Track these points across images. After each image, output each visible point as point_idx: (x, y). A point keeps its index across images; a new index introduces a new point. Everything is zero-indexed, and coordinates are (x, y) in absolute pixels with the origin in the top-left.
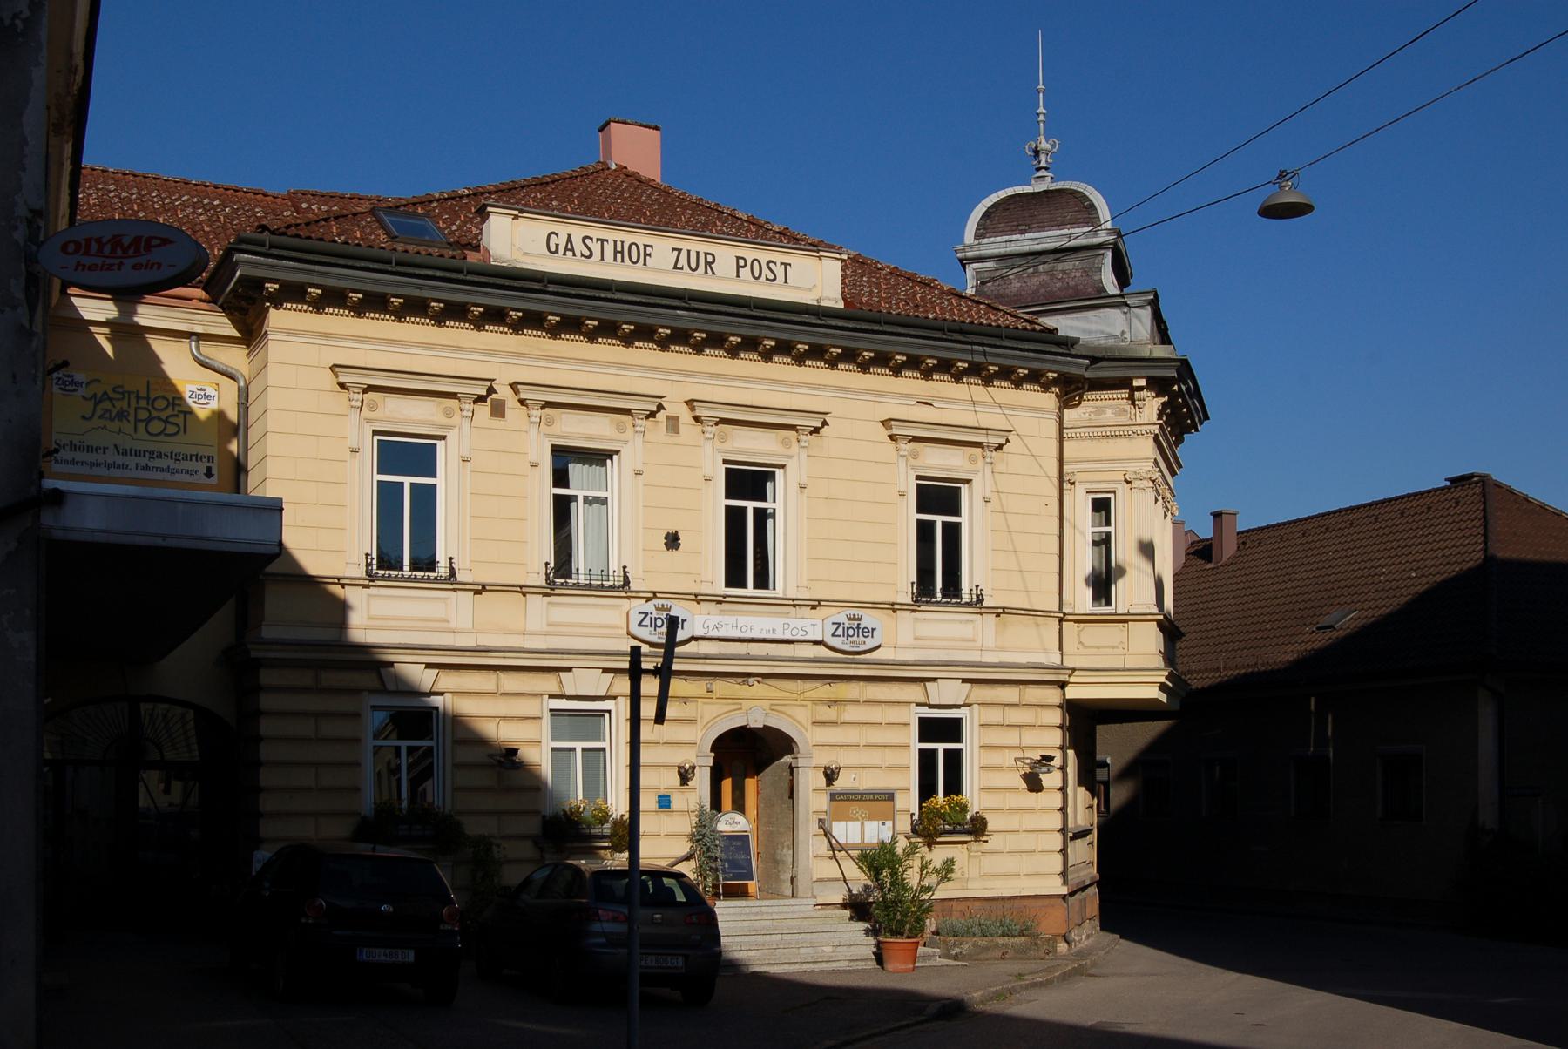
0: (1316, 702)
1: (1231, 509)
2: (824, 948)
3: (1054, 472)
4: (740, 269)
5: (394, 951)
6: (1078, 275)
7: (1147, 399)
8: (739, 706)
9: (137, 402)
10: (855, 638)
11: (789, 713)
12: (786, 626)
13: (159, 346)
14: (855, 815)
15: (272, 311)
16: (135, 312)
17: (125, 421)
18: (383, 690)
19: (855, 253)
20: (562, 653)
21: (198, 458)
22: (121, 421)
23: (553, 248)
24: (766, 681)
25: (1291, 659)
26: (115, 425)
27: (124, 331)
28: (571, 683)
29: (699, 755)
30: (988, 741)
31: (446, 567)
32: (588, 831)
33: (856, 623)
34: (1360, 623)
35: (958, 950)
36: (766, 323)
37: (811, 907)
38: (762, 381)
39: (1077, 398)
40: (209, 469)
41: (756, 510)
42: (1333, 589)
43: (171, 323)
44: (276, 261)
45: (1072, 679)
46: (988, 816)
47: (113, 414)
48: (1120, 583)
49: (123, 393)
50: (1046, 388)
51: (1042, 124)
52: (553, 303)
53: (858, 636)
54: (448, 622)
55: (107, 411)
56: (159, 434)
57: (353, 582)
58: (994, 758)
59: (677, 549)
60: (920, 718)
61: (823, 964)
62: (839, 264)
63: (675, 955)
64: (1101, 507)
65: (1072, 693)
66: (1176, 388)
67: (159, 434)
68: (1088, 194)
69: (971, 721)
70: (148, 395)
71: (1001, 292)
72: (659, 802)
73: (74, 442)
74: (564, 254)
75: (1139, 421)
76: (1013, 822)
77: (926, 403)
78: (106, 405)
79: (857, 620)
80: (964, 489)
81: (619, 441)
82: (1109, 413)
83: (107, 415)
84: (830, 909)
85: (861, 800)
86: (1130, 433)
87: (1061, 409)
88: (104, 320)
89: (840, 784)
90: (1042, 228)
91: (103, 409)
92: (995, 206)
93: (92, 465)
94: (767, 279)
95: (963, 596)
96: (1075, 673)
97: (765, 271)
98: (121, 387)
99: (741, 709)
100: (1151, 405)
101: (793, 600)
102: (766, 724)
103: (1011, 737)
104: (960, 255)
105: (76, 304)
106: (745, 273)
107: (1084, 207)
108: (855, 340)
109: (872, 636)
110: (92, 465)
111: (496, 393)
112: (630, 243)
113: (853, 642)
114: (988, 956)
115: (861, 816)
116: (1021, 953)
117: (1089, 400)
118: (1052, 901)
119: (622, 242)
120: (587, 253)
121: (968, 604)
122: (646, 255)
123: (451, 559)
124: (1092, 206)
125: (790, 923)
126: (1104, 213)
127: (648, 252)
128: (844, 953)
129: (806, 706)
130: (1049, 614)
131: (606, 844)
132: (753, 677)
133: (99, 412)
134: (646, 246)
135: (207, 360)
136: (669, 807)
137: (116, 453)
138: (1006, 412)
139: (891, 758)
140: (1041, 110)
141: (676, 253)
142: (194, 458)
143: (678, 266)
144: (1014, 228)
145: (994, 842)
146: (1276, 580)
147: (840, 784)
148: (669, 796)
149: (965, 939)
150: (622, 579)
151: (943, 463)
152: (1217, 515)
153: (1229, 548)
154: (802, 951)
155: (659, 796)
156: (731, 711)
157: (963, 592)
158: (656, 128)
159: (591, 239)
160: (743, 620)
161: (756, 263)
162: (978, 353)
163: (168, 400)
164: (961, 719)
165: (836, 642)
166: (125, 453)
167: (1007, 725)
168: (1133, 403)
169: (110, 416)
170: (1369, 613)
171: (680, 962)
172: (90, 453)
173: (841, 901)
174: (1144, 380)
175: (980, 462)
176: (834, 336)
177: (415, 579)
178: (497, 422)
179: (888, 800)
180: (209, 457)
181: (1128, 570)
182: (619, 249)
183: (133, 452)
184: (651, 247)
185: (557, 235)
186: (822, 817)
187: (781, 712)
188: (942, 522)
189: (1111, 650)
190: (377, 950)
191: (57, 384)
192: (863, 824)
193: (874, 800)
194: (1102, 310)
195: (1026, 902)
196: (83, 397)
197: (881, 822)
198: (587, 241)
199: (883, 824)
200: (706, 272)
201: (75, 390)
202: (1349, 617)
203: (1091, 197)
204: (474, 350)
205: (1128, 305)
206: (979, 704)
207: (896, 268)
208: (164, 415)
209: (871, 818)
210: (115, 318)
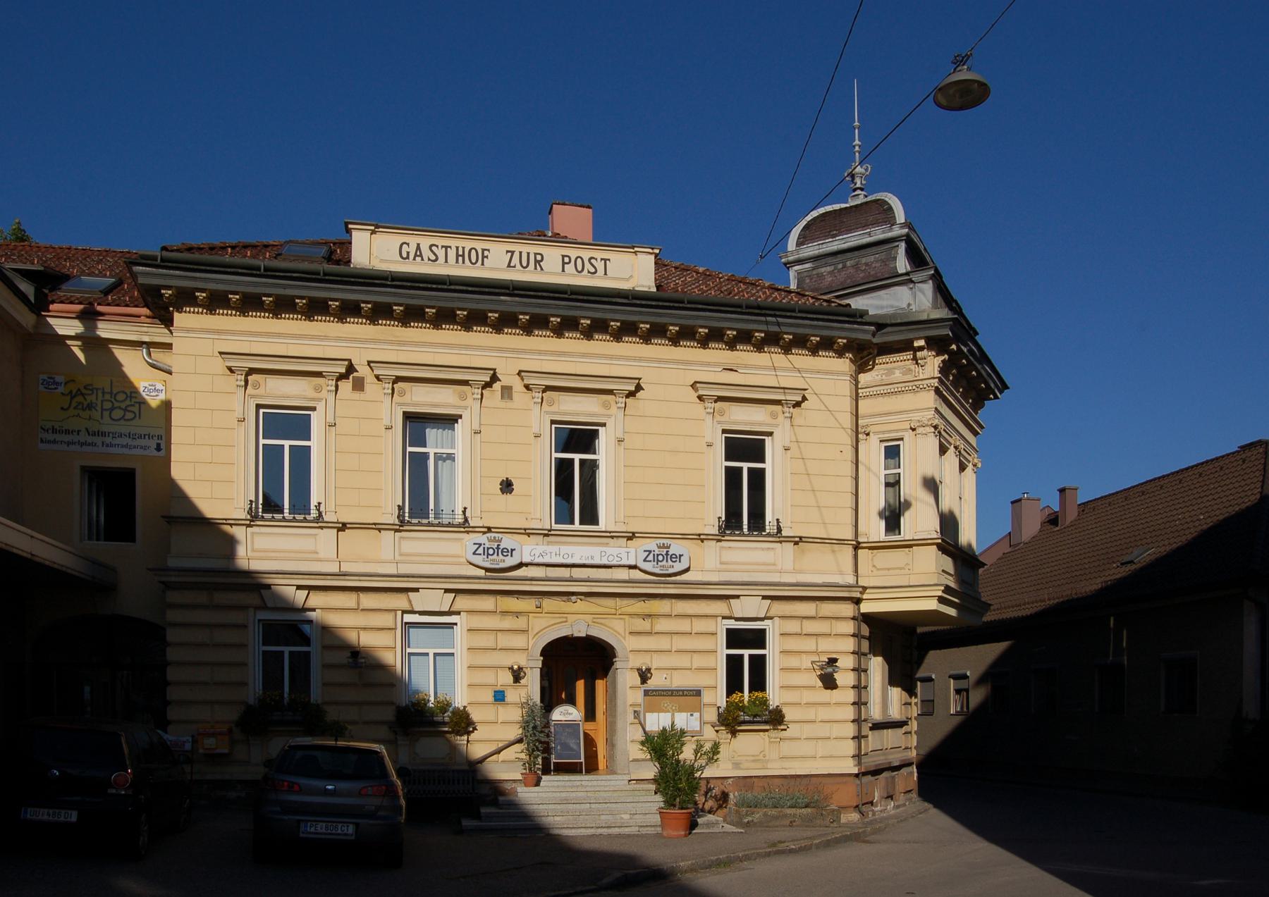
0: (1115, 620)
1: (1074, 486)
2: (623, 816)
3: (847, 421)
4: (566, 265)
5: (57, 811)
6: (878, 265)
7: (929, 358)
8: (565, 620)
9: (103, 396)
11: (607, 624)
13: (120, 354)
14: (666, 708)
15: (176, 315)
16: (96, 327)
17: (93, 410)
18: (264, 607)
19: (704, 269)
20: (408, 577)
21: (150, 437)
22: (91, 410)
23: (405, 255)
24: (588, 599)
25: (1097, 588)
26: (86, 414)
27: (94, 344)
28: (739, 608)
32: (431, 718)
33: (665, 550)
34: (1153, 557)
35: (750, 819)
36: (579, 304)
38: (584, 355)
39: (871, 363)
40: (159, 445)
41: (582, 462)
42: (1139, 534)
43: (118, 334)
44: (164, 271)
45: (865, 596)
46: (785, 710)
47: (85, 406)
48: (907, 514)
49: (92, 390)
50: (840, 354)
51: (857, 154)
52: (395, 294)
53: (667, 561)
54: (317, 553)
55: (79, 403)
56: (119, 420)
57: (236, 523)
58: (793, 662)
59: (510, 493)
60: (727, 629)
61: (616, 829)
62: (653, 257)
63: (344, 823)
64: (892, 453)
65: (866, 608)
66: (954, 347)
67: (119, 420)
68: (887, 199)
69: (772, 630)
70: (111, 390)
71: (816, 286)
72: (495, 696)
73: (55, 427)
74: (414, 259)
75: (921, 377)
76: (810, 714)
77: (731, 370)
78: (80, 399)
79: (666, 548)
80: (768, 440)
81: (460, 407)
83: (80, 407)
84: (644, 784)
85: (672, 695)
86: (914, 387)
88: (74, 334)
89: (653, 683)
90: (849, 231)
91: (77, 402)
92: (814, 219)
93: (69, 444)
94: (589, 272)
96: (868, 591)
97: (587, 265)
98: (91, 385)
99: (566, 622)
100: (932, 364)
101: (610, 532)
102: (588, 633)
103: (809, 644)
104: (783, 260)
105: (51, 323)
106: (570, 268)
107: (884, 210)
108: (660, 316)
109: (680, 562)
110: (69, 444)
111: (357, 371)
113: (663, 566)
114: (777, 823)
115: (671, 708)
116: (808, 822)
117: (881, 364)
118: (845, 779)
119: (463, 248)
120: (433, 257)
121: (769, 535)
122: (483, 257)
124: (890, 208)
125: (602, 794)
126: (900, 216)
127: (485, 255)
128: (639, 819)
129: (624, 619)
130: (843, 542)
131: (446, 729)
132: (576, 595)
133: (74, 404)
134: (483, 250)
135: (155, 363)
136: (504, 701)
137: (87, 434)
138: (804, 375)
139: (698, 661)
140: (857, 142)
141: (510, 254)
142: (147, 437)
143: (512, 265)
144: (827, 234)
145: (793, 730)
146: (1100, 533)
147: (653, 683)
148: (504, 691)
149: (755, 809)
151: (746, 418)
152: (1062, 491)
153: (1072, 515)
154: (603, 817)
155: (495, 692)
156: (555, 624)
158: (589, 207)
159: (437, 246)
160: (565, 549)
161: (579, 260)
162: (772, 324)
163: (126, 393)
164: (765, 629)
165: (648, 567)
166: (94, 434)
167: (805, 635)
168: (917, 363)
169: (83, 407)
170: (1162, 549)
171: (351, 829)
172: (67, 435)
173: (653, 777)
174: (923, 341)
175: (781, 417)
176: (641, 313)
177: (294, 520)
178: (357, 395)
180: (158, 436)
181: (913, 502)
182: (461, 253)
183: (100, 433)
184: (489, 250)
185: (408, 244)
186: (636, 709)
187: (601, 624)
189: (887, 571)
190: (42, 810)
191: (42, 384)
192: (673, 715)
193: (683, 695)
194: (892, 289)
195: (820, 779)
196: (62, 393)
197: (689, 714)
198: (434, 248)
199: (692, 715)
200: (536, 268)
201: (56, 389)
202: (1148, 553)
203: (889, 202)
204: (338, 339)
205: (912, 282)
206: (779, 617)
207: (733, 275)
208: (123, 405)
209: (680, 711)
210: (82, 333)
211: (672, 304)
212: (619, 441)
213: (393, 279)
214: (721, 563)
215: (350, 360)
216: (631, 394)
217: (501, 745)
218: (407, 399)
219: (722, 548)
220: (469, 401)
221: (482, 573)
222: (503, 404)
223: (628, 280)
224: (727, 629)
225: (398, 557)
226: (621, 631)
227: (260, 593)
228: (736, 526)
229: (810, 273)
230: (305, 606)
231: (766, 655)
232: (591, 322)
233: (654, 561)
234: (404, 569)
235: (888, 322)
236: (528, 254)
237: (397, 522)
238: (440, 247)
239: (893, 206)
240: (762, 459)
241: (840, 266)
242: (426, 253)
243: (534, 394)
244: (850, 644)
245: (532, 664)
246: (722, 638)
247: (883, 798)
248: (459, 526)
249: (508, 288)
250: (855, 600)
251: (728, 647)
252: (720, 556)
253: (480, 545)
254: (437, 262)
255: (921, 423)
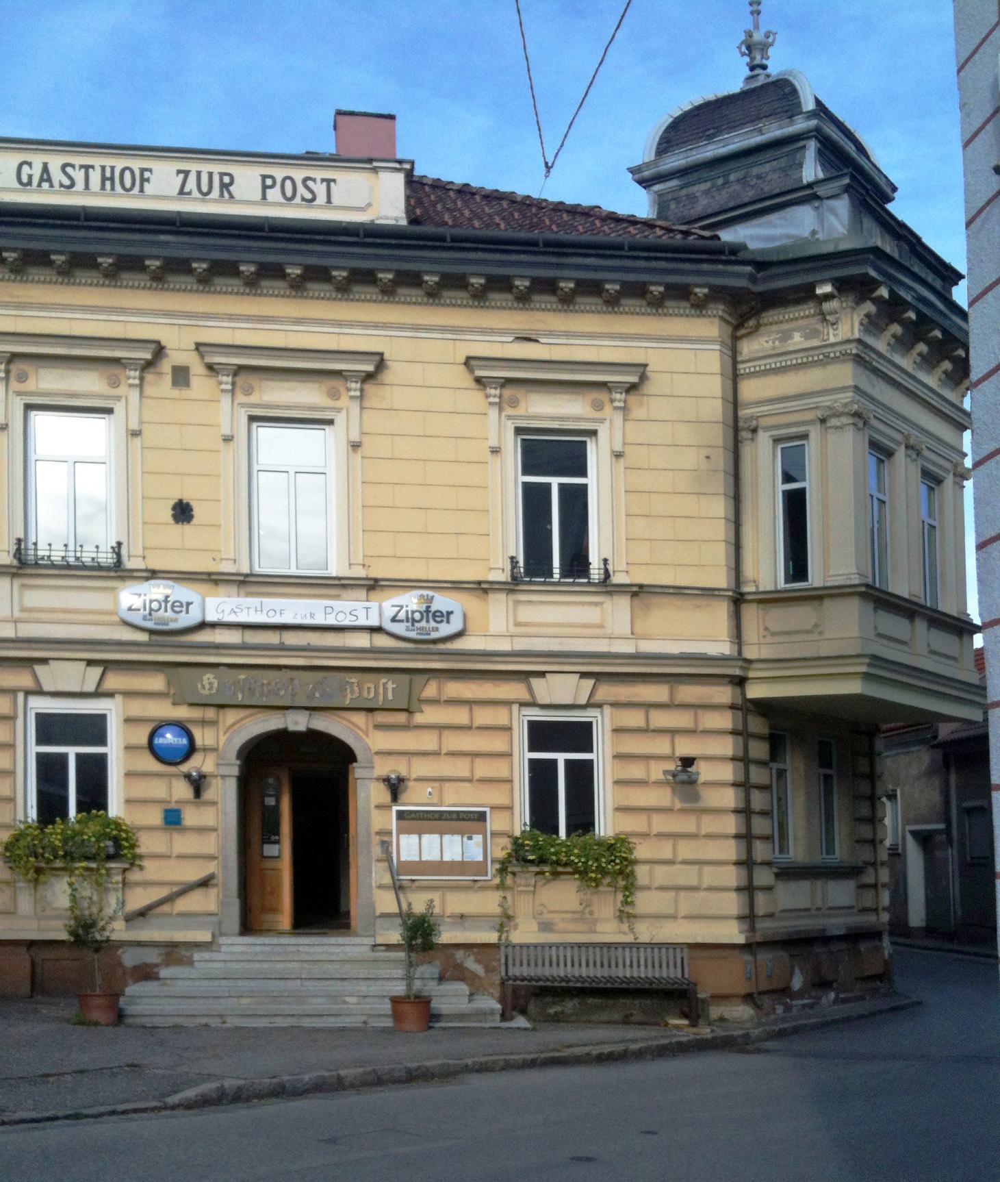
6: (775, 176)
10: (423, 624)
12: (329, 610)
23: (25, 179)
28: (546, 690)
29: (221, 762)
30: (624, 749)
31: (599, 569)
37: (367, 949)
38: (298, 321)
45: (751, 674)
50: (700, 307)
58: (635, 771)
65: (755, 691)
69: (602, 724)
74: (39, 185)
75: (832, 340)
76: (665, 851)
81: (331, 409)
82: (797, 337)
85: (440, 819)
87: (735, 339)
95: (592, 571)
97: (301, 190)
103: (661, 746)
106: (274, 195)
112: (122, 167)
119: (113, 168)
120: (67, 182)
123: (605, 561)
134: (143, 170)
141: (181, 176)
144: (701, 134)
150: (602, 572)
157: (591, 567)
164: (591, 723)
165: (399, 629)
168: (824, 320)
179: (476, 820)
182: (108, 174)
185: (30, 164)
188: (560, 484)
211: (421, 243)
212: (353, 446)
213: (87, 219)
214: (517, 624)
215: (382, 354)
216: (369, 377)
217: (175, 889)
218: (520, 411)
219: (517, 602)
220: (344, 401)
221: (143, 637)
222: (175, 393)
223: (361, 209)
224: (530, 722)
225: (17, 614)
226: (363, 726)
227: (33, 668)
228: (579, 571)
229: (675, 195)
230: (100, 690)
231: (592, 760)
232: (622, 287)
233: (408, 621)
234: (27, 631)
235: (775, 259)
236: (211, 175)
237: (15, 562)
238: (77, 168)
239: (798, 87)
240: (582, 471)
241: (720, 181)
242: (57, 175)
243: (220, 378)
244: (726, 747)
245: (224, 770)
246: (521, 736)
247: (813, 985)
248: (108, 569)
249: (358, 235)
250: (737, 680)
251: (532, 748)
252: (515, 615)
253: (402, 607)
254: (74, 189)
255: (833, 411)
